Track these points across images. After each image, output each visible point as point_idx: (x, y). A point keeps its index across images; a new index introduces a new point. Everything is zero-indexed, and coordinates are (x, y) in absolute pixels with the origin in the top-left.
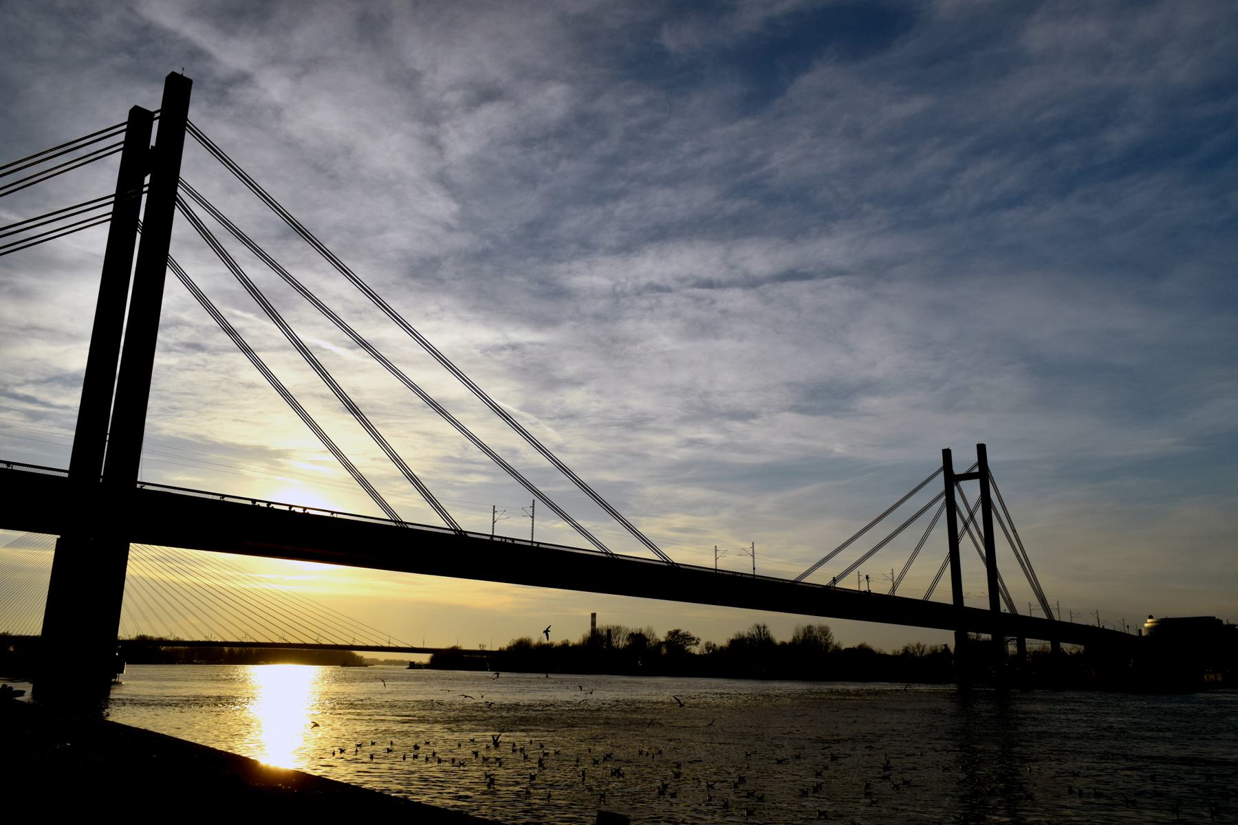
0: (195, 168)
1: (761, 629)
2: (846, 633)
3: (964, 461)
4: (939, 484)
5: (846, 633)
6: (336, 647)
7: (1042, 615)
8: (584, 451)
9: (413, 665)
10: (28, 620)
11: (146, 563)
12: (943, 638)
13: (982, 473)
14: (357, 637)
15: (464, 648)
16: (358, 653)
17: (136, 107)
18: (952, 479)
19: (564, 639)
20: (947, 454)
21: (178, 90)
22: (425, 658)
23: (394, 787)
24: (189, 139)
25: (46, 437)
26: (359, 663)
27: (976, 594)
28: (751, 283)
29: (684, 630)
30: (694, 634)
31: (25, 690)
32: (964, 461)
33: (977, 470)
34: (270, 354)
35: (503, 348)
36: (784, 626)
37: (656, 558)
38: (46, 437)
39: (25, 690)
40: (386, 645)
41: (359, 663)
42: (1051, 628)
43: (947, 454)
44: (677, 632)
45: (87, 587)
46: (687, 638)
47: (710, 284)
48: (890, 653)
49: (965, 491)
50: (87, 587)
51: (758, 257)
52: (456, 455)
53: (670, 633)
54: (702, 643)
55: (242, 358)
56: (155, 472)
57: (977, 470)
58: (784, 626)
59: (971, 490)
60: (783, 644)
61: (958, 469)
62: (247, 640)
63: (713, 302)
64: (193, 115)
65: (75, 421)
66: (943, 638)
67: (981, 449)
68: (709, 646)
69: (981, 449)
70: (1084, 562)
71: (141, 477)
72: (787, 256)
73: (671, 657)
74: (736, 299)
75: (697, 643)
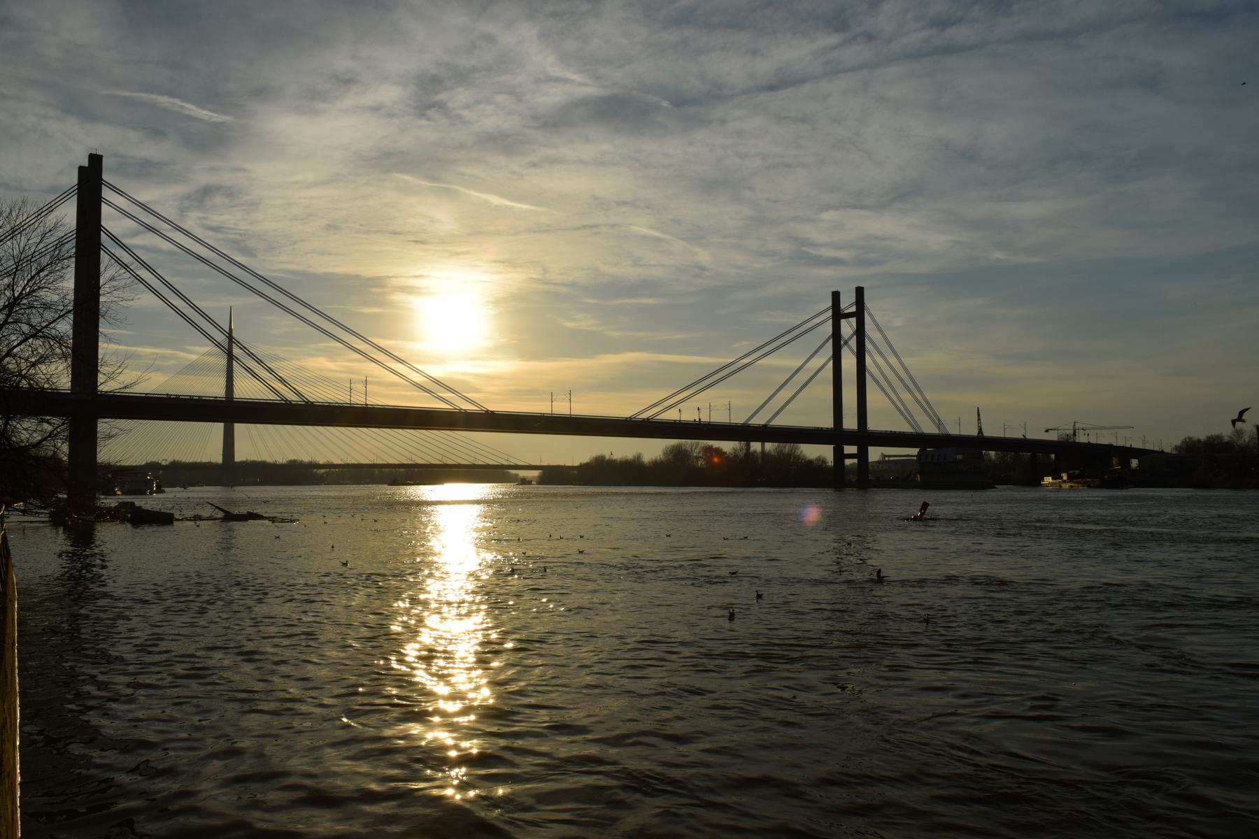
1: (680, 446)
3: (848, 303)
13: (859, 314)
14: (447, 454)
20: (836, 296)
43: (836, 296)
57: (853, 309)
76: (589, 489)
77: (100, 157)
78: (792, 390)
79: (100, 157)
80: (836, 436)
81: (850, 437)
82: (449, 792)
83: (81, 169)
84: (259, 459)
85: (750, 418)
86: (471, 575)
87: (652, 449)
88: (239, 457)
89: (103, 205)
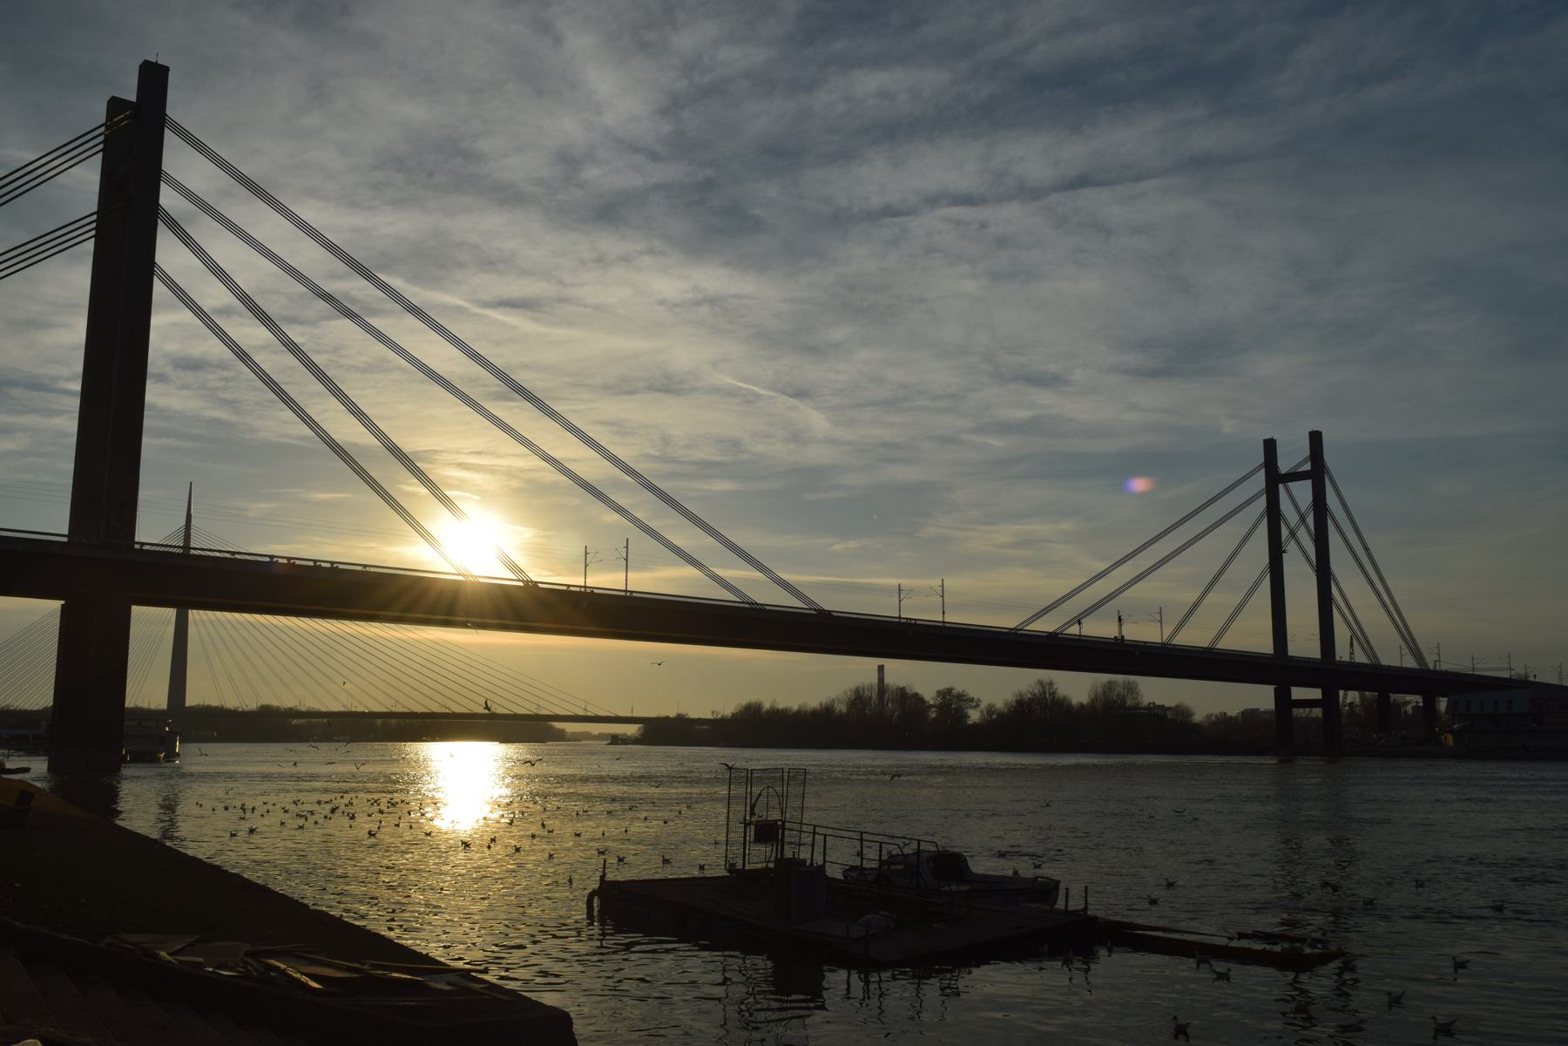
0: (177, 159)
1: (1045, 686)
2: (1156, 691)
3: (1292, 456)
4: (1260, 480)
5: (1156, 691)
6: (515, 717)
7: (1410, 662)
8: (831, 441)
9: (615, 740)
10: (37, 693)
13: (1317, 471)
14: (542, 703)
15: (693, 715)
17: (113, 98)
18: (1275, 479)
20: (1270, 446)
21: (154, 78)
22: (632, 730)
24: (170, 138)
25: (49, 516)
26: (560, 736)
27: (1304, 641)
28: (1029, 193)
29: (959, 688)
30: (972, 693)
31: (38, 767)
32: (1292, 456)
33: (1308, 467)
35: (697, 303)
36: (1077, 687)
39: (38, 767)
40: (581, 713)
41: (560, 736)
42: (1428, 681)
43: (1270, 446)
44: (949, 691)
45: (92, 655)
46: (962, 698)
47: (968, 200)
49: (1296, 491)
50: (92, 655)
51: (1033, 154)
52: (653, 452)
53: (939, 693)
54: (983, 706)
55: (347, 323)
56: (154, 527)
57: (1308, 467)
58: (1077, 687)
59: (1303, 491)
60: (1082, 706)
61: (1284, 466)
62: (399, 709)
63: (983, 225)
64: (173, 110)
65: (146, 413)
66: (1261, 697)
67: (1316, 438)
68: (991, 710)
69: (1316, 438)
70: (1443, 591)
72: (1076, 152)
73: (945, 726)
74: (1011, 216)
75: (977, 706)
76: (1112, 760)
77: (164, 71)
78: (1207, 593)
79: (164, 71)
80: (1273, 667)
81: (1303, 672)
82: (163, 954)
83: (115, 105)
84: (215, 703)
85: (1219, 637)
86: (1390, 1006)
87: (992, 687)
88: (192, 699)
89: (164, 187)
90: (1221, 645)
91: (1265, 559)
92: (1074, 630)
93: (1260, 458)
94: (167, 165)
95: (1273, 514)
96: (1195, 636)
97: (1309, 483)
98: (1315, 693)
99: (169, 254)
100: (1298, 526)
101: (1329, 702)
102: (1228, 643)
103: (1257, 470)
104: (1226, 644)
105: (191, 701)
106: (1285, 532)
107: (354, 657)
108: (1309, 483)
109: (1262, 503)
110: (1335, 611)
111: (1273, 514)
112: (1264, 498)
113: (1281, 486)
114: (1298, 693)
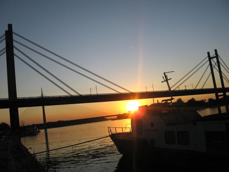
0: (15, 37)
2: (198, 97)
3: (212, 54)
4: (208, 59)
11: (22, 111)
12: (213, 96)
13: (217, 56)
16: (106, 118)
18: (210, 58)
19: (129, 110)
20: (208, 53)
21: (10, 26)
22: (116, 117)
23: (27, 138)
25: (5, 95)
27: (219, 86)
32: (212, 54)
33: (215, 56)
34: (204, 87)
37: (128, 92)
38: (5, 95)
43: (208, 53)
45: (14, 116)
48: (196, 100)
50: (14, 116)
57: (215, 56)
59: (215, 60)
61: (211, 56)
66: (213, 96)
67: (216, 51)
69: (216, 51)
71: (18, 97)
77: (11, 25)
79: (11, 25)
81: (220, 90)
83: (6, 31)
90: (204, 88)
91: (210, 71)
92: (178, 89)
93: (207, 55)
94: (14, 38)
95: (211, 64)
96: (199, 87)
97: (216, 58)
98: (222, 94)
99: (15, 52)
100: (215, 65)
101: (224, 95)
102: (205, 87)
103: (207, 57)
104: (204, 88)
105: (47, 122)
106: (213, 67)
107: (73, 112)
108: (216, 58)
109: (208, 63)
110: (223, 78)
111: (211, 64)
112: (209, 61)
113: (211, 60)
114: (219, 94)
